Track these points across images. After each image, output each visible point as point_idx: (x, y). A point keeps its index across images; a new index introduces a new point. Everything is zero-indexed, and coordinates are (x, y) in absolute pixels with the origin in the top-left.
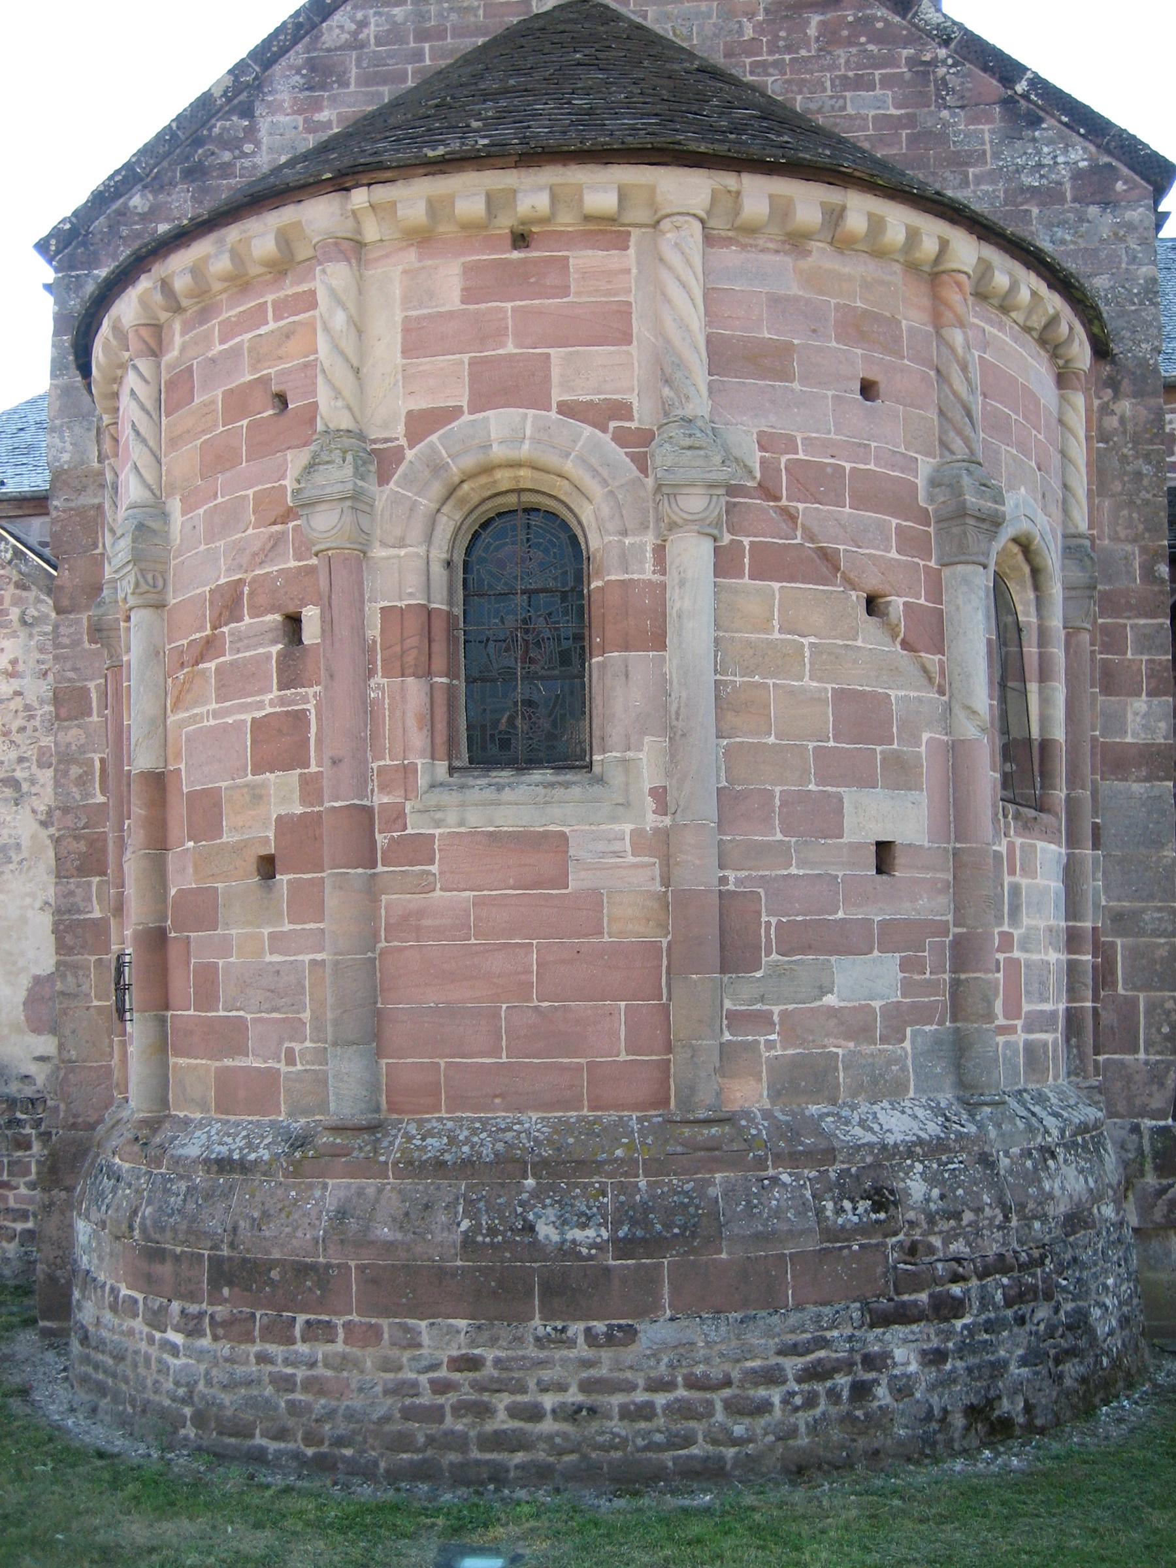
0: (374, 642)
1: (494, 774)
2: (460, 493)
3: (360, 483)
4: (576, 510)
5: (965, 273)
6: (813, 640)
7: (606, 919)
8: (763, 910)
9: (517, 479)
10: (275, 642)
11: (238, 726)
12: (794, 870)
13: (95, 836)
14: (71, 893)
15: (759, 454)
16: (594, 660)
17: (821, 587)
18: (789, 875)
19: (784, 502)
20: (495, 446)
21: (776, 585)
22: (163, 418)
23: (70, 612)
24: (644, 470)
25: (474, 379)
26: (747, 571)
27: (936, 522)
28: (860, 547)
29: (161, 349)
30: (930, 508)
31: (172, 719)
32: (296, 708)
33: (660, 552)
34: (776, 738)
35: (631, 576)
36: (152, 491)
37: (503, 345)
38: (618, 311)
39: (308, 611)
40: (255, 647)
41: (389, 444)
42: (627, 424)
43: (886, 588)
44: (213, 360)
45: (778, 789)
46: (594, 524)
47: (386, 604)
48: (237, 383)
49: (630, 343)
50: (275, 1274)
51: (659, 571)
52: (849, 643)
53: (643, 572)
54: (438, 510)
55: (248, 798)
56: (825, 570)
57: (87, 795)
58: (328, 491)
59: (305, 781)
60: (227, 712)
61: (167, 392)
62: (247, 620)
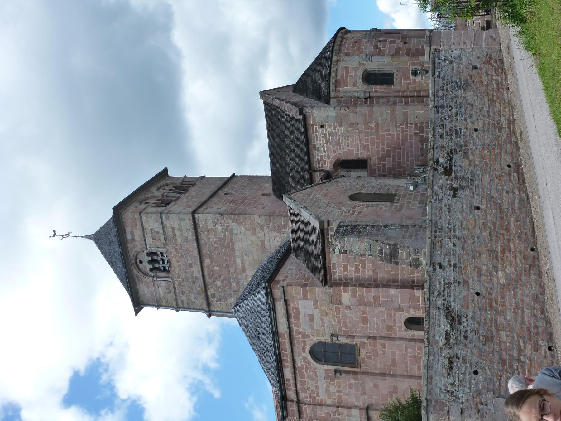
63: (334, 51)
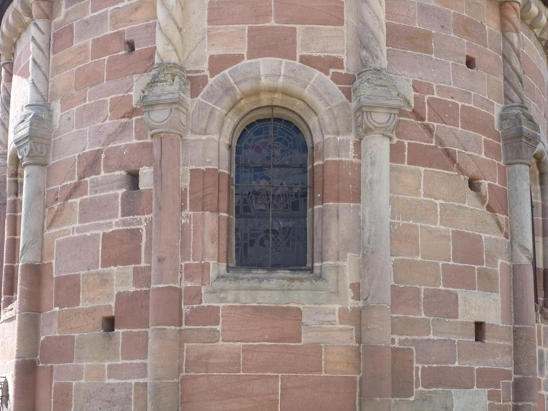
0: (186, 189)
1: (255, 272)
2: (239, 105)
3: (182, 95)
4: (306, 120)
5: (518, 3)
6: (442, 202)
7: (323, 362)
8: (415, 360)
9: (272, 99)
10: (121, 187)
11: (94, 237)
12: (431, 337)
15: (413, 93)
16: (315, 207)
17: (446, 172)
18: (429, 340)
19: (426, 122)
20: (263, 80)
21: (422, 169)
22: (51, 55)
24: (349, 98)
25: (251, 39)
26: (406, 160)
27: (503, 140)
28: (466, 150)
29: (52, 15)
30: (500, 132)
31: (47, 233)
32: (133, 227)
33: (358, 145)
34: (422, 258)
35: (341, 159)
36: (42, 96)
37: (269, 21)
38: (336, 6)
39: (143, 170)
40: (108, 190)
41: (199, 74)
42: (340, 71)
43: (480, 175)
44: (87, 22)
45: (423, 288)
46: (318, 128)
47: (194, 167)
48: (102, 35)
49: (342, 24)
51: (357, 157)
52: (461, 204)
53: (348, 156)
54: (226, 115)
55: (98, 281)
56: (448, 161)
58: (163, 98)
59: (137, 272)
60: (87, 229)
61: (54, 40)
62: (103, 174)
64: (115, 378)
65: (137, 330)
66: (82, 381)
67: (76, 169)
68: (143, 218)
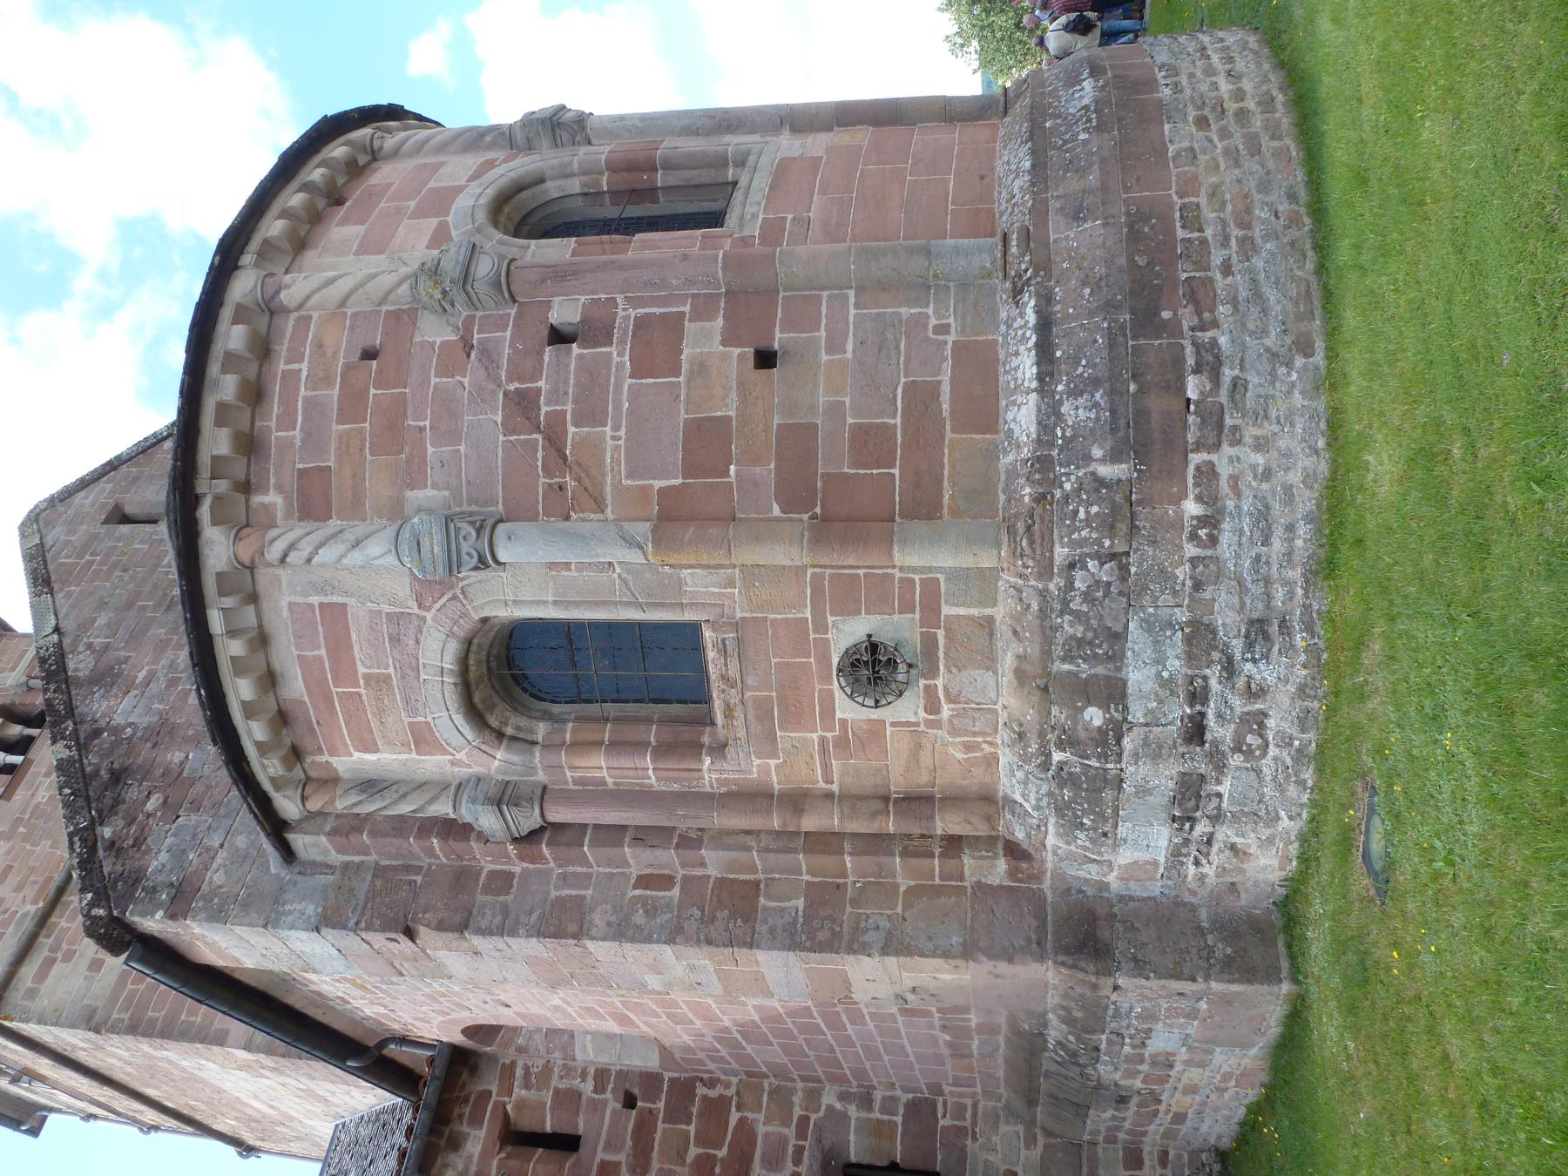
13: (715, 899)
14: (772, 931)
23: (471, 913)
50: (1141, 261)
57: (669, 905)
59: (697, 316)
63: (203, 485)
64: (846, 341)
65: (780, 310)
66: (847, 401)
67: (522, 437)
68: (621, 313)
